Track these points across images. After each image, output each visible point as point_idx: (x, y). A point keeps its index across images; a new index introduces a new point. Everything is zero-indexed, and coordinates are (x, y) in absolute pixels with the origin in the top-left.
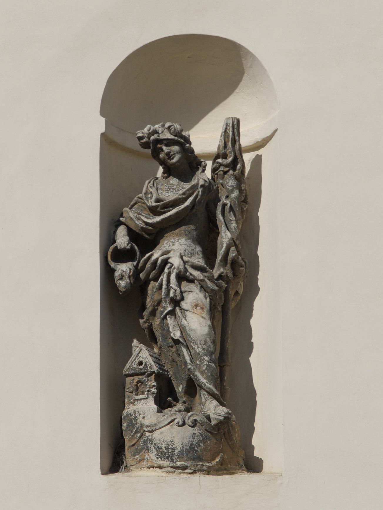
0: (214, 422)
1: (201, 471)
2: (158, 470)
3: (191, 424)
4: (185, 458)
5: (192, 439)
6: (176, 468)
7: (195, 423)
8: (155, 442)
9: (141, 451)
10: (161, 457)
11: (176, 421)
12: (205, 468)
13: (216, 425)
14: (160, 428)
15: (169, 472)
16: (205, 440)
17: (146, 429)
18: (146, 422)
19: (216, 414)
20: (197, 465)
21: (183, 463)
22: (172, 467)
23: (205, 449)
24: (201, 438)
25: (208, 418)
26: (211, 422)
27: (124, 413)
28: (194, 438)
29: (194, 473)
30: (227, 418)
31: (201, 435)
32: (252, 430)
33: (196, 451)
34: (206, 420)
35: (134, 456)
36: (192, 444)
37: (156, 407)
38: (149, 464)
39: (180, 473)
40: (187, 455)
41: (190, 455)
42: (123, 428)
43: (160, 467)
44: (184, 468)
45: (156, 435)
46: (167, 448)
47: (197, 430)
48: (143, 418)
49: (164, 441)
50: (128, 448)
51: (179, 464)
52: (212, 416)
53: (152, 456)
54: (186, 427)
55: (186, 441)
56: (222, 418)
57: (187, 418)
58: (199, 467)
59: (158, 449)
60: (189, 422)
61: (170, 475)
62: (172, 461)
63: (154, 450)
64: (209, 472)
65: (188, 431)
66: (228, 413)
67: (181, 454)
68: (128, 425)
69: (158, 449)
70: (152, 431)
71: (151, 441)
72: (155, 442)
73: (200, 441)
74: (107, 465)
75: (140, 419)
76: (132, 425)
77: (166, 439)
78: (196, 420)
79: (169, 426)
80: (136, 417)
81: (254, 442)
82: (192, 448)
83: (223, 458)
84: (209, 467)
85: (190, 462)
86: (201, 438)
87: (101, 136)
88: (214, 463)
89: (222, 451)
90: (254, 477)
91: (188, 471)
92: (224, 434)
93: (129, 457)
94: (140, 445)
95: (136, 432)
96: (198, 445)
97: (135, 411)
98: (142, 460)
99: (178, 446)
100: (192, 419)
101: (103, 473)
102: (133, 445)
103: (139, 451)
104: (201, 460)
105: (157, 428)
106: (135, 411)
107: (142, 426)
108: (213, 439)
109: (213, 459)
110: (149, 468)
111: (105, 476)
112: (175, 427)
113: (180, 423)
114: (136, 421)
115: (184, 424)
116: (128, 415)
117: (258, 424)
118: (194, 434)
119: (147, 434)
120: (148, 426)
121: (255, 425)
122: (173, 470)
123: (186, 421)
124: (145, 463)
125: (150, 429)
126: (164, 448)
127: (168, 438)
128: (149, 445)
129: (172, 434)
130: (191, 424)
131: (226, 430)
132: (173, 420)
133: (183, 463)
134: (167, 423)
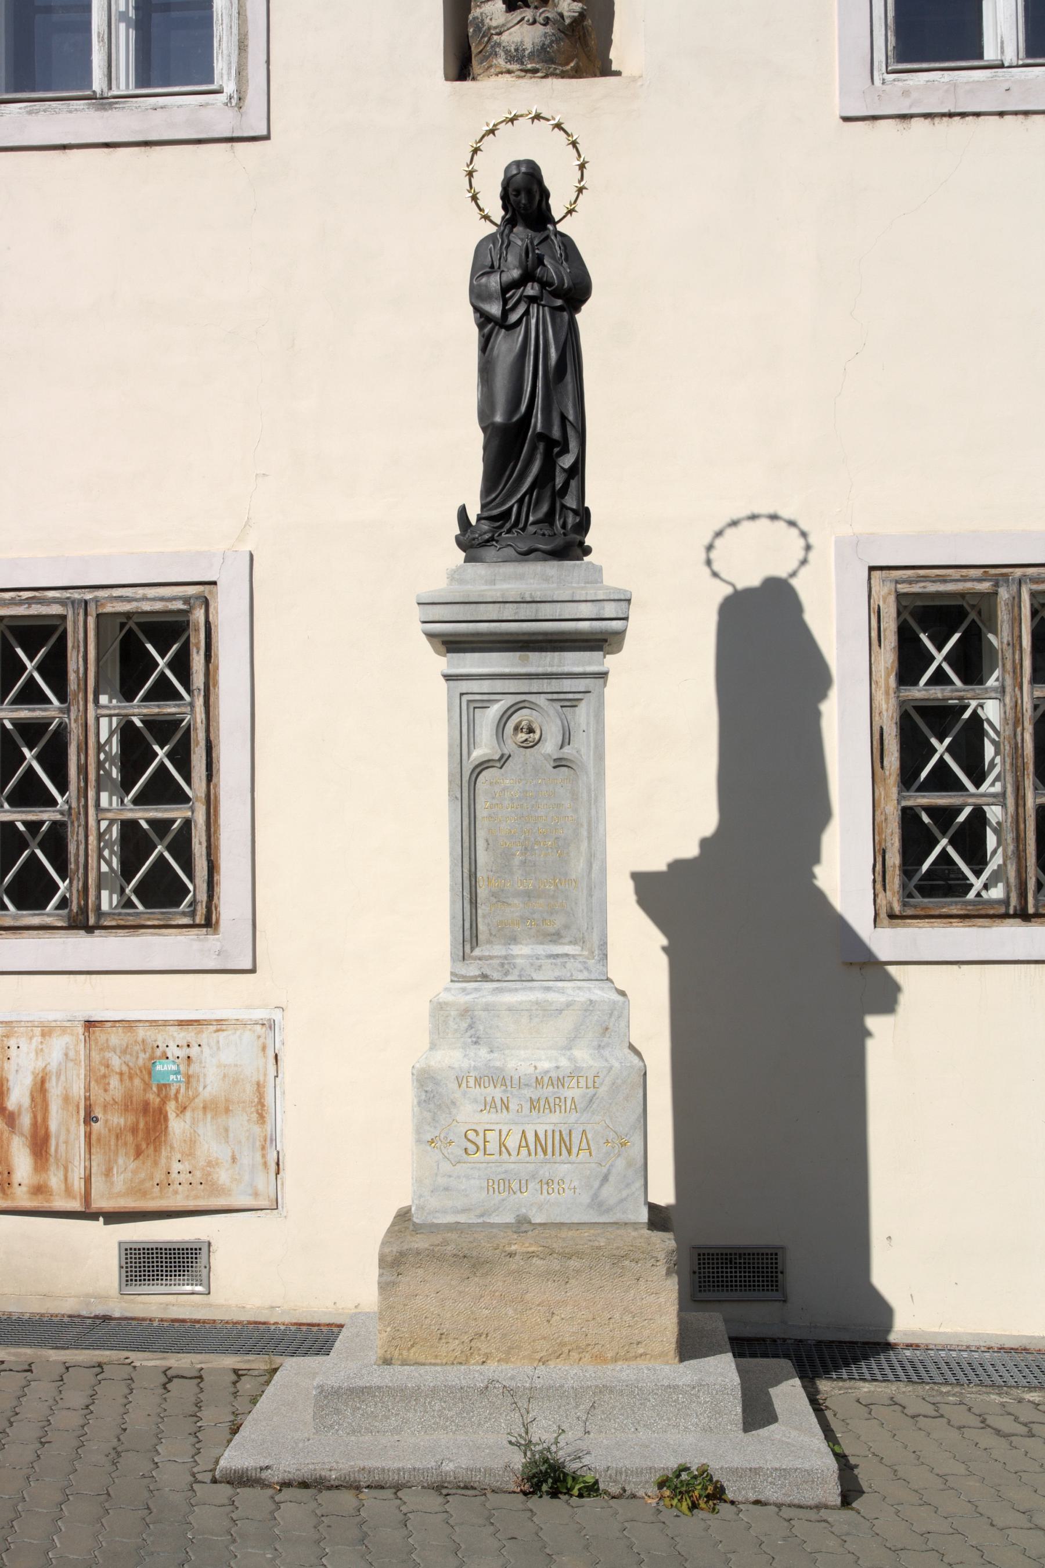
0: (567, 21)
1: (554, 75)
2: (507, 75)
3: (542, 22)
4: (536, 59)
5: (543, 39)
6: (527, 71)
7: (547, 22)
8: (503, 44)
9: (488, 57)
10: (510, 61)
11: (526, 19)
12: (558, 71)
13: (571, 24)
14: (508, 29)
15: (519, 77)
16: (558, 41)
17: (494, 32)
18: (494, 23)
19: (569, 11)
20: (550, 68)
21: (534, 65)
22: (521, 70)
23: (558, 51)
24: (554, 38)
25: (561, 15)
26: (564, 20)
27: (470, 17)
28: (546, 37)
29: (545, 77)
30: (582, 15)
31: (554, 35)
32: (609, 42)
33: (548, 52)
34: (559, 18)
35: (481, 63)
36: (544, 44)
37: (504, 6)
38: (498, 70)
39: (531, 78)
40: (538, 56)
41: (542, 56)
42: (470, 34)
43: (509, 72)
44: (535, 71)
45: (505, 37)
46: (516, 50)
47: (549, 29)
48: (491, 19)
49: (513, 42)
50: (476, 56)
51: (529, 66)
52: (566, 14)
53: (501, 62)
54: (537, 25)
55: (537, 41)
56: (576, 14)
57: (538, 14)
58: (551, 70)
59: (507, 52)
60: (541, 19)
61: (521, 81)
62: (522, 63)
63: (502, 54)
64: (563, 75)
65: (539, 29)
66: (582, 8)
67: (532, 53)
68: (474, 31)
69: (507, 52)
70: (500, 34)
71: (499, 44)
72: (503, 44)
73: (552, 42)
74: (454, 71)
75: (487, 21)
76: (478, 29)
77: (515, 40)
78: (547, 18)
79: (518, 26)
80: (482, 20)
81: (612, 56)
82: (543, 48)
83: (577, 63)
84: (562, 71)
85: (541, 64)
86: (554, 38)
87: (541, 177)
88: (568, 67)
89: (576, 56)
90: (610, 674)
91: (539, 74)
92: (579, 38)
93: (476, 67)
94: (487, 51)
95: (484, 36)
96: (550, 45)
97: (481, 14)
98: (490, 67)
99: (529, 46)
100: (543, 16)
101: (447, 78)
102: (481, 52)
103: (486, 58)
104: (553, 63)
105: (506, 28)
106: (481, 14)
107: (489, 28)
108: (567, 41)
109: (567, 64)
110: (497, 75)
111: (449, 83)
112: (525, 26)
113: (531, 21)
114: (483, 25)
115: (534, 22)
116: (474, 18)
117: (616, 36)
118: (546, 33)
119: (495, 37)
120: (496, 28)
121: (613, 37)
122: (523, 74)
123: (537, 18)
124: (492, 70)
125: (498, 30)
126: (513, 50)
127: (517, 39)
128: (497, 50)
129: (522, 34)
130: (542, 22)
131: (581, 34)
132: (522, 19)
133: (534, 65)
134: (516, 22)
